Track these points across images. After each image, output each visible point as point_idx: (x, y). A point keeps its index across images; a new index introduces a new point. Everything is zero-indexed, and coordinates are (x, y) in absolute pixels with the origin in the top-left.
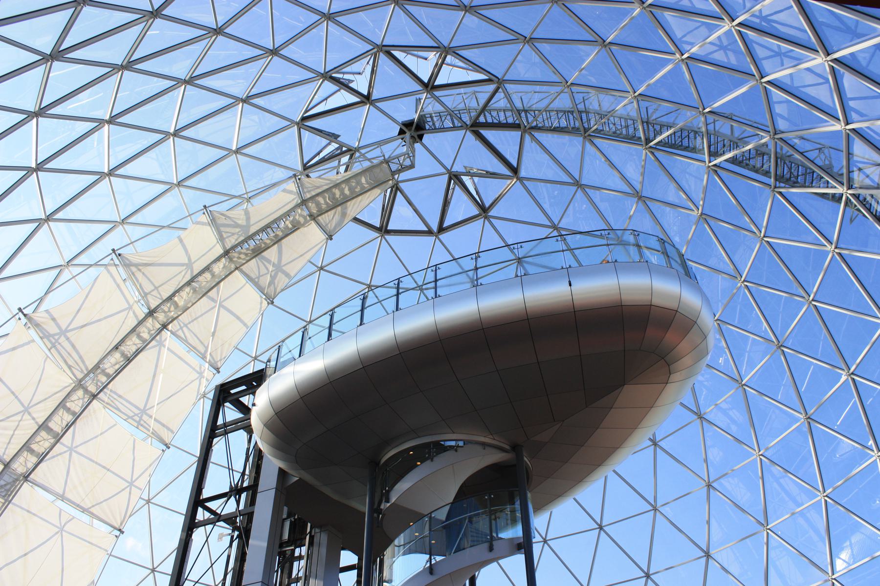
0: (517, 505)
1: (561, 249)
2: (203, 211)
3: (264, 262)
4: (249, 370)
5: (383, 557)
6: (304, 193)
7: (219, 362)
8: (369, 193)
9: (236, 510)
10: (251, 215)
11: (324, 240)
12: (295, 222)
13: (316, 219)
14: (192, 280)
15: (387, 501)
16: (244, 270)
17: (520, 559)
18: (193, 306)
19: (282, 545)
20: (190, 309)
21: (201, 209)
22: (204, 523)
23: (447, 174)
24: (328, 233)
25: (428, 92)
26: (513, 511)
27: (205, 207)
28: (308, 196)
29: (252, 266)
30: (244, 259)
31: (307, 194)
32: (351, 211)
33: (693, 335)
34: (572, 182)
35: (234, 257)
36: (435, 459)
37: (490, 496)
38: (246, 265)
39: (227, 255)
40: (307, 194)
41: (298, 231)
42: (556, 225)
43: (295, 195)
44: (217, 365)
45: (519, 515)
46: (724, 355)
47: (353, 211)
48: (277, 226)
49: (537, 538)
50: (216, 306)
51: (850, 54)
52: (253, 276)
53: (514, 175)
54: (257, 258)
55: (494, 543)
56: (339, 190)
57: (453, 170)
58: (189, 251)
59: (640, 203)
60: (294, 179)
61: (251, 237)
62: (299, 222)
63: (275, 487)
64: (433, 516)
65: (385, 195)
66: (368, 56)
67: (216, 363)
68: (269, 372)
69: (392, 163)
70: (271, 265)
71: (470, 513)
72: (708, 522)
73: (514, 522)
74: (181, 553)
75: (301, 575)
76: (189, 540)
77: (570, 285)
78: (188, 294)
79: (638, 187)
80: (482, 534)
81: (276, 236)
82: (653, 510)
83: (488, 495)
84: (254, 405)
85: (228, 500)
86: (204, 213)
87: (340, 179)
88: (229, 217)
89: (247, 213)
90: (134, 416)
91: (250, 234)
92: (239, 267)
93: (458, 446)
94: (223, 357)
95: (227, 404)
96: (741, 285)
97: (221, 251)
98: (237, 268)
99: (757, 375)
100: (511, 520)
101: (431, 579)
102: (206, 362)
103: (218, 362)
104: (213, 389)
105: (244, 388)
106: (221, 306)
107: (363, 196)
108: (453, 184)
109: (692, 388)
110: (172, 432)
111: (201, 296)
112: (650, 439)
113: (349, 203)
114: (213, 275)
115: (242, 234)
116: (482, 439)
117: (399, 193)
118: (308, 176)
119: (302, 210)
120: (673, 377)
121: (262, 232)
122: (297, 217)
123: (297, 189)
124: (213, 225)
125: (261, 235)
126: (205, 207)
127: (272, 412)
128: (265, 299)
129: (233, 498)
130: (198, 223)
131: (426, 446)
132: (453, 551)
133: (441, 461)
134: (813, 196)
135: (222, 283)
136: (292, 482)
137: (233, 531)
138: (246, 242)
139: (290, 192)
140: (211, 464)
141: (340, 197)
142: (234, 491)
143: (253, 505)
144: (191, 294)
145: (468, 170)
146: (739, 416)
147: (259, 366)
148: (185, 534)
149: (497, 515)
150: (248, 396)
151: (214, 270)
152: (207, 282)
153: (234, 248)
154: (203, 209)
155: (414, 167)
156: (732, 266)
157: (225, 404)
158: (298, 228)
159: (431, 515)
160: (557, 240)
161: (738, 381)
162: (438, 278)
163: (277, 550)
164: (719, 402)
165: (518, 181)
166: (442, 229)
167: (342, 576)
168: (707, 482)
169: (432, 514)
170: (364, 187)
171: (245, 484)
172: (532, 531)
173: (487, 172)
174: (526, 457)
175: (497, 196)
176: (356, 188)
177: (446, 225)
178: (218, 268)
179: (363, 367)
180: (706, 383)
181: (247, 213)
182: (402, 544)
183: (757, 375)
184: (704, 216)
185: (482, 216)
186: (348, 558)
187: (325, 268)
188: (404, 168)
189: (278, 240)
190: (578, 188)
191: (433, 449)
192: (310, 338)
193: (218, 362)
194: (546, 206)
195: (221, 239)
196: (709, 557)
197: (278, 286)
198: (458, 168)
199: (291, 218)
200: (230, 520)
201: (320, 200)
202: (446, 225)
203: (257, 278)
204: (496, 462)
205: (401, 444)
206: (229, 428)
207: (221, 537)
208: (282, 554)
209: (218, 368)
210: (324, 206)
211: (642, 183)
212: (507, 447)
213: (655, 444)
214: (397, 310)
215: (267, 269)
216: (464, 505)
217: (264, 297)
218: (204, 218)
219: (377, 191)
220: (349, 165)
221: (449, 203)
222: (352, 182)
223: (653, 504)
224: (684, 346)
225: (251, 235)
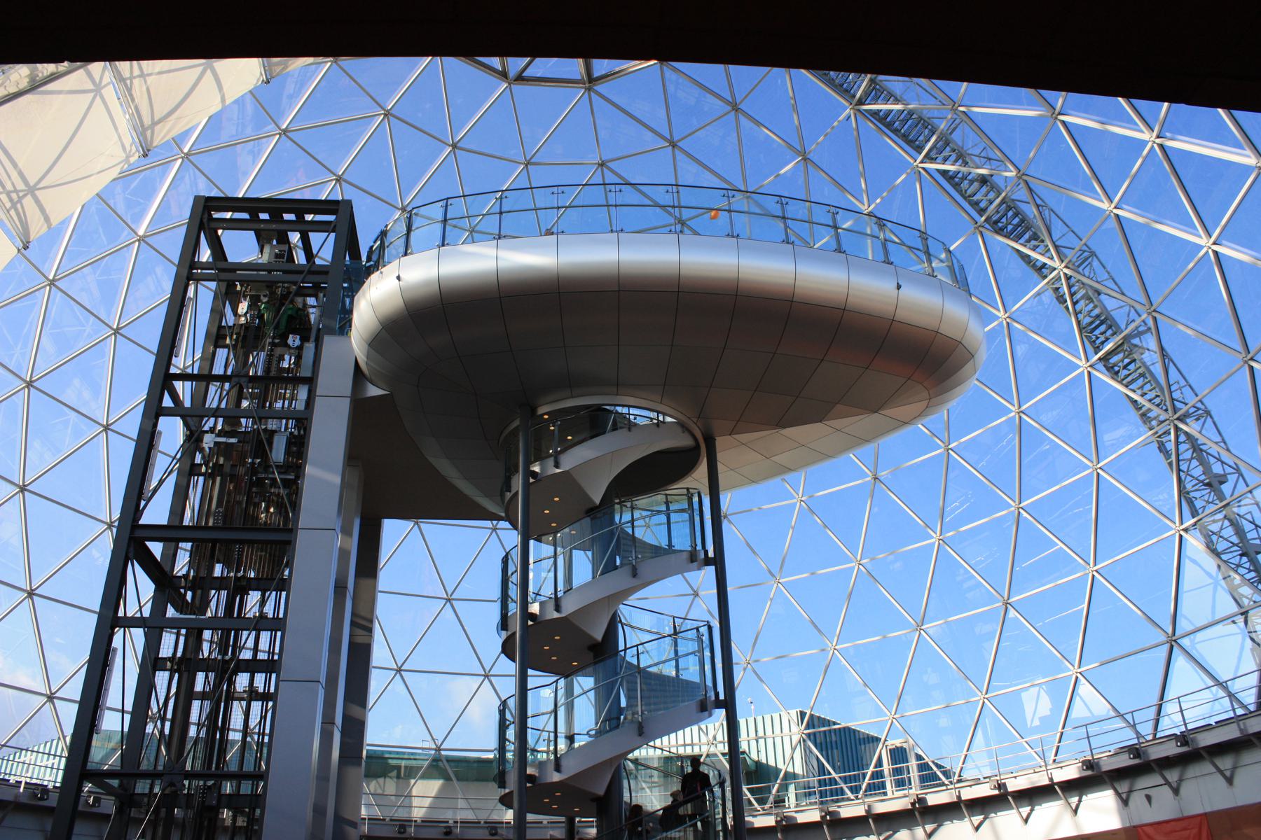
17: (711, 570)
90: (11, 192)
134: (1016, 256)
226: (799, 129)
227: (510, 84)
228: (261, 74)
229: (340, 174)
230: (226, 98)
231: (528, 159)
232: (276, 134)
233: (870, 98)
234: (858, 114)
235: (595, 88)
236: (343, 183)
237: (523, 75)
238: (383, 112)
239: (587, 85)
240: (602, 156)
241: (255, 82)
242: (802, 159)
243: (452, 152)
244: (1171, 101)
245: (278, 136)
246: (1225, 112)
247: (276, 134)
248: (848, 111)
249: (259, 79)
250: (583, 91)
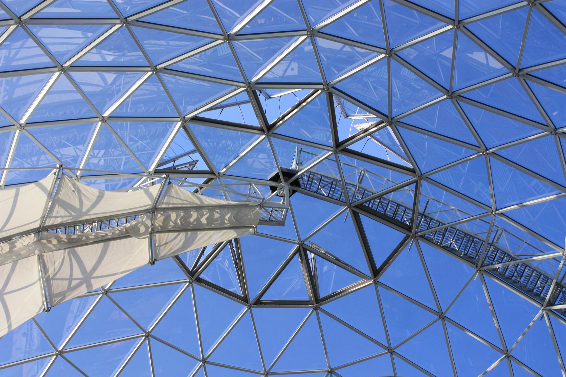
25: (335, 152)
41: (128, 239)
51: (91, 128)
53: (373, 277)
66: (313, 89)
107: (216, 231)
155: (284, 226)
158: (130, 237)
166: (259, 302)
185: (312, 306)
198: (315, 243)
201: (173, 216)
222: (217, 212)
226: (500, 330)
227: (250, 307)
228: (43, 304)
229: (150, 330)
230: (12, 324)
231: (267, 370)
232: (54, 355)
233: (558, 300)
234: (550, 313)
236: (150, 338)
237: (261, 299)
238: (144, 334)
239: (315, 305)
240: (331, 365)
241: (38, 310)
242: (506, 357)
243: (203, 366)
245: (55, 357)
247: (54, 355)
248: (541, 312)
249: (41, 308)
250: (312, 310)
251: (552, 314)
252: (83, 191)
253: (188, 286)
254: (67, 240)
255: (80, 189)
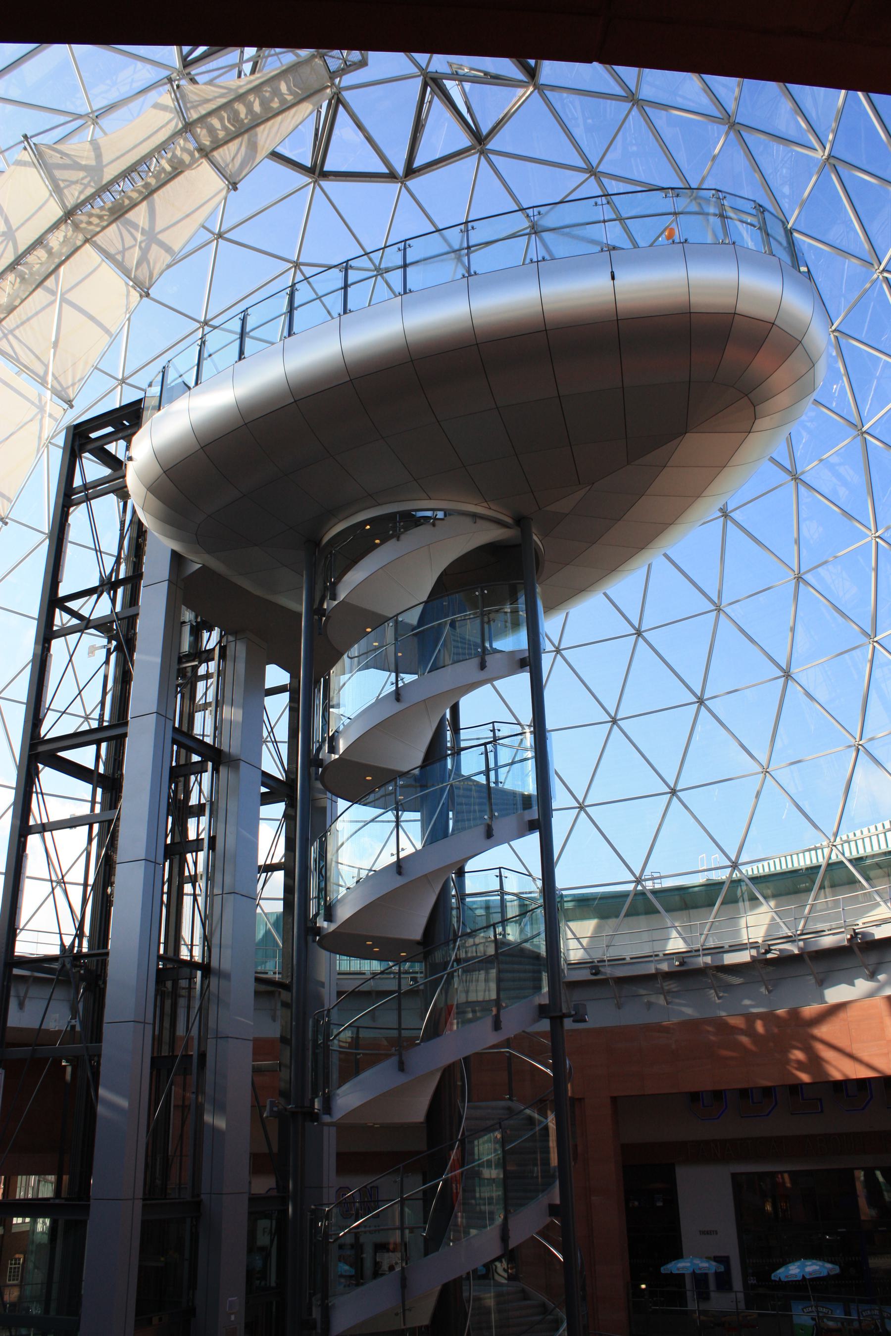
0: (522, 600)
1: (602, 219)
2: (22, 145)
3: (128, 227)
4: (114, 402)
5: (329, 678)
6: (187, 109)
7: (71, 389)
8: (293, 111)
9: (112, 612)
10: (103, 150)
11: (221, 190)
12: (176, 161)
13: (209, 156)
14: (17, 261)
15: (334, 598)
16: (99, 242)
18: (24, 303)
19: (181, 660)
20: (18, 309)
21: (18, 141)
22: (65, 632)
23: (419, 76)
24: (228, 176)
26: (515, 612)
27: (25, 137)
28: (194, 115)
29: (111, 236)
30: (97, 225)
31: (192, 111)
32: (265, 142)
33: (795, 362)
34: (624, 94)
35: (82, 222)
36: (402, 537)
37: (482, 591)
38: (101, 234)
39: (69, 218)
40: (192, 111)
42: (594, 166)
43: (171, 112)
44: (67, 393)
45: (523, 614)
46: (841, 381)
47: (268, 142)
48: (147, 169)
49: (547, 646)
50: (55, 301)
52: (112, 251)
53: (530, 81)
54: (118, 222)
55: (488, 658)
56: (244, 105)
57: (430, 69)
58: (5, 209)
59: (732, 135)
60: (168, 87)
61: (106, 188)
62: (181, 162)
63: (167, 578)
64: (400, 619)
65: (319, 112)
67: (65, 389)
68: (150, 403)
69: (330, 56)
70: (138, 231)
71: (453, 615)
72: (793, 629)
73: (516, 625)
74: (38, 667)
75: (211, 700)
76: (47, 654)
77: (613, 278)
78: (14, 285)
79: (731, 107)
80: (470, 645)
81: (147, 185)
82: (716, 610)
83: (479, 590)
84: (130, 459)
85: (98, 598)
86: (25, 149)
87: (244, 85)
88: (67, 155)
89: (94, 143)
91: (104, 182)
92: (91, 238)
93: (435, 519)
94: (77, 379)
95: (87, 455)
96: (878, 277)
97: (60, 213)
98: (87, 241)
99: (885, 418)
100: (511, 623)
101: (398, 707)
102: (48, 389)
103: (68, 388)
104: (63, 430)
105: (110, 429)
106: (63, 300)
108: (430, 93)
109: (787, 439)
110: (9, 500)
111: (34, 286)
112: (721, 510)
113: (260, 129)
114: (50, 252)
115: (90, 182)
116: (472, 508)
117: (341, 108)
118: (193, 81)
119: (186, 140)
120: (760, 424)
121: (124, 179)
122: (178, 152)
123: (176, 103)
124: (40, 164)
125: (122, 184)
126: (25, 137)
127: (157, 470)
128: (133, 287)
129: (105, 595)
130: (19, 163)
131: (391, 517)
132: (427, 671)
133: (412, 539)
135: (62, 269)
136: (192, 571)
137: (109, 642)
138: (99, 196)
139: (164, 108)
140: (69, 544)
141: (246, 118)
142: (106, 584)
143: (134, 605)
144: (17, 285)
145: (454, 70)
146: (854, 476)
147: (131, 396)
148: (41, 647)
149: (492, 616)
150: (115, 443)
151: (51, 244)
152: (40, 264)
153: (79, 206)
154: (23, 142)
156: (866, 246)
157: (84, 455)
159: (397, 618)
160: (596, 204)
161: (857, 427)
162: (408, 261)
163: (175, 666)
164: (825, 457)
165: (536, 91)
166: (411, 171)
167: (269, 701)
168: (796, 573)
169: (399, 616)
170: (285, 99)
171: (122, 575)
172: (541, 636)
173: (486, 74)
174: (536, 534)
175: (501, 117)
176: (272, 100)
177: (417, 163)
178: (55, 240)
179: (295, 401)
180: (809, 424)
181: (94, 143)
182: (356, 655)
183: (885, 418)
184: (832, 161)
186: (276, 675)
187: (225, 236)
188: (350, 65)
189: (149, 193)
190: (633, 105)
191: (400, 522)
192: (210, 356)
193: (68, 388)
194: (578, 132)
195: (57, 190)
196: (789, 678)
197: (154, 268)
199: (169, 155)
200: (103, 626)
201: (215, 122)
202: (417, 163)
203: (119, 253)
204: (491, 541)
205: (351, 515)
206: (92, 491)
207: (92, 650)
208: (181, 673)
209: (70, 401)
210: (221, 134)
211: (738, 100)
212: (509, 520)
213: (725, 514)
214: (345, 312)
215: (135, 239)
216: (444, 603)
217: (131, 283)
218: (26, 156)
219: (306, 108)
220: (257, 62)
221: (423, 126)
222: (266, 91)
223: (717, 602)
224: (780, 376)
225: (106, 184)
227: (402, 183)
235: (488, 147)
239: (479, 148)
244: (848, 88)
246: (863, 94)
251: (650, 106)
252: (73, 153)
253: (314, 188)
254: (108, 212)
255: (65, 151)
